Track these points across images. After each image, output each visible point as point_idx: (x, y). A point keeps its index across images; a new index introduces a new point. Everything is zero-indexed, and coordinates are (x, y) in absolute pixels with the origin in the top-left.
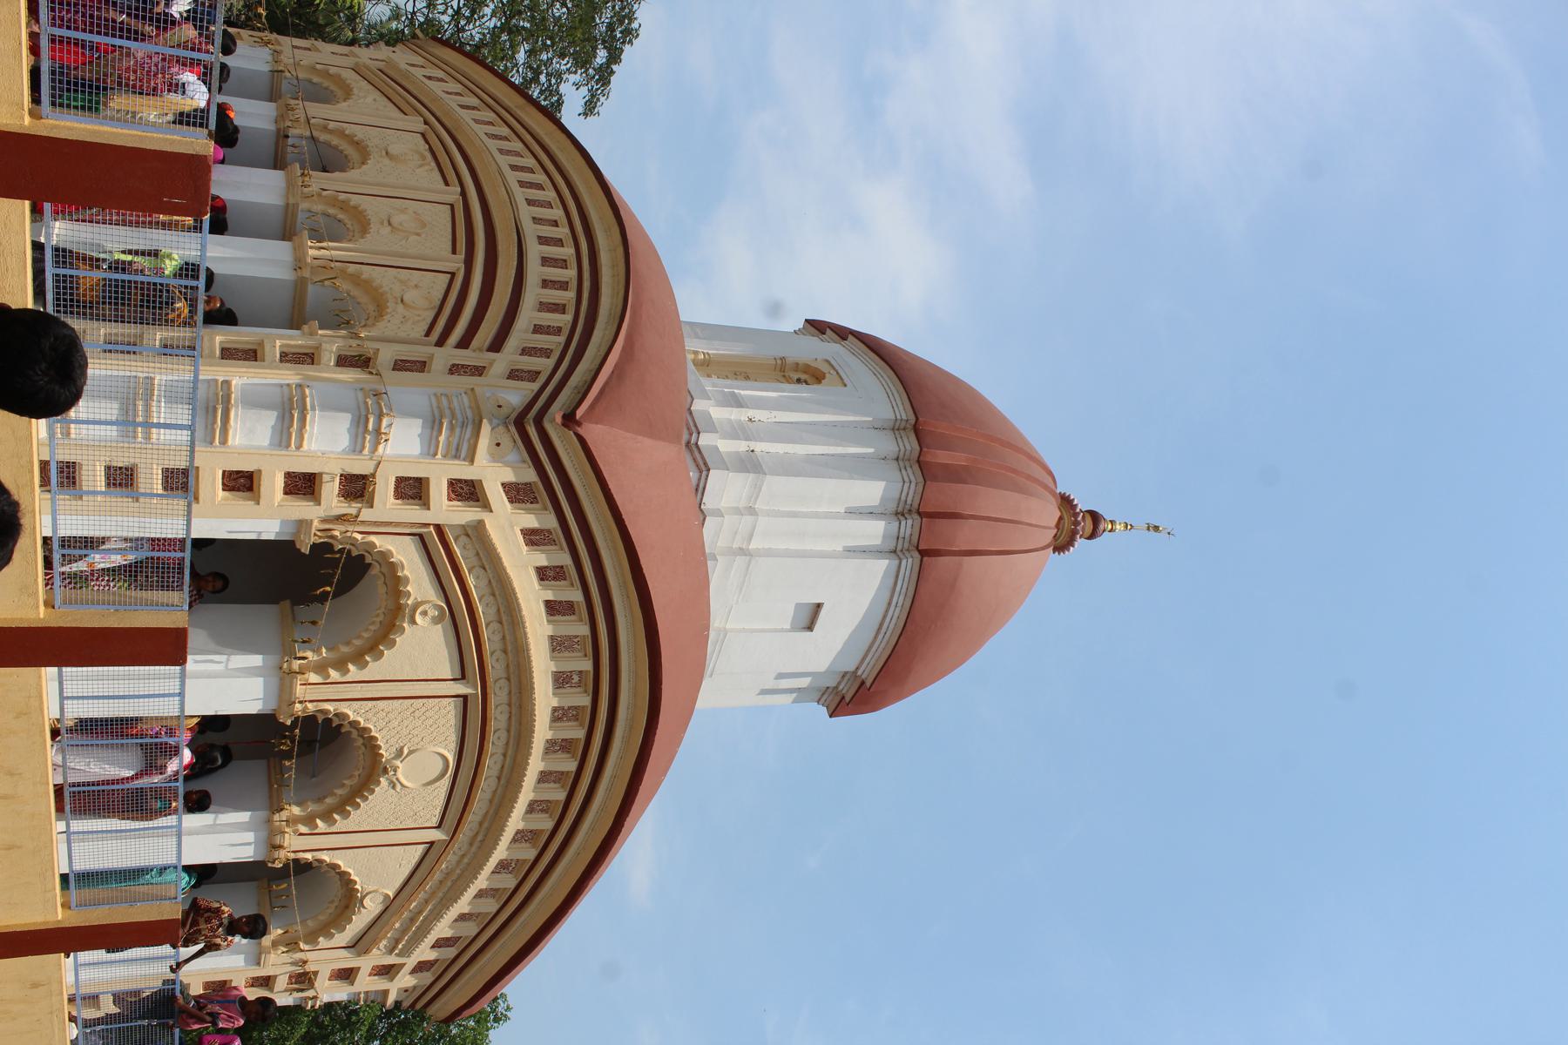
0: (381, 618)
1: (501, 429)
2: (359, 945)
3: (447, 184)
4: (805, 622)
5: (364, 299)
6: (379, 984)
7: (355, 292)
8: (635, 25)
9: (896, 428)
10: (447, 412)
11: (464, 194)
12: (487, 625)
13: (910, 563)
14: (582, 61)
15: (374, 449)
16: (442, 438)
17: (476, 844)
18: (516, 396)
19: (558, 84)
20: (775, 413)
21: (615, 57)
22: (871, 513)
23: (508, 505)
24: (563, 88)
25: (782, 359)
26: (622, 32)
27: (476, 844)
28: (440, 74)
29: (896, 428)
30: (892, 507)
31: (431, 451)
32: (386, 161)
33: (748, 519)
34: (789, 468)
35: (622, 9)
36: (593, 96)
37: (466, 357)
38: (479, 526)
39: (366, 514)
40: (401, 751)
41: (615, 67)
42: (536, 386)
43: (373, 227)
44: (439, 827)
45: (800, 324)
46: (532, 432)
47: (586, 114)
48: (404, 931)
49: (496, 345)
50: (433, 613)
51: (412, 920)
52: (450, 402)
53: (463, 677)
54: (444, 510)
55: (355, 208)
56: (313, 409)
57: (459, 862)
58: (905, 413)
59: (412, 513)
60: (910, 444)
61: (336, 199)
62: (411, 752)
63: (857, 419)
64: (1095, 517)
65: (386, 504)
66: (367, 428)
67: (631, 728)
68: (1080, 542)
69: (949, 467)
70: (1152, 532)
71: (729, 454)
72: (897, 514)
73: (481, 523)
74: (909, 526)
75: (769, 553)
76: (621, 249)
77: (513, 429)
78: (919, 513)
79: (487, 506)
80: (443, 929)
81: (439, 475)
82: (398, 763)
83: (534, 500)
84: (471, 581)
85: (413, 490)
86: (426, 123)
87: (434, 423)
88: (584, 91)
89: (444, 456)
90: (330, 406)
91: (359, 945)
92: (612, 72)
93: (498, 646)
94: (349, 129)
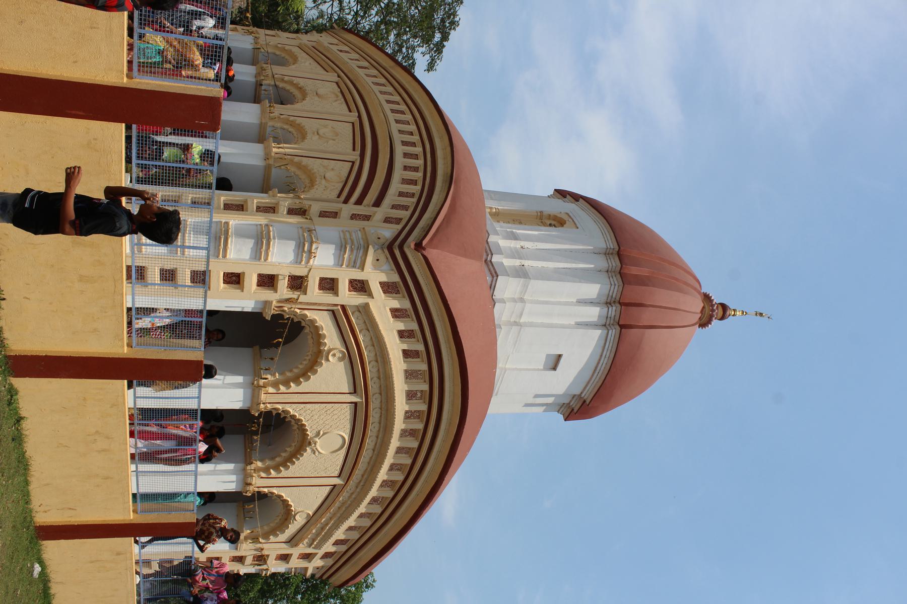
0: (309, 357)
1: (380, 251)
2: (292, 541)
3: (350, 111)
5: (303, 177)
7: (298, 172)
8: (457, 19)
9: (607, 253)
10: (349, 241)
11: (360, 117)
13: (614, 332)
14: (427, 40)
15: (308, 262)
16: (346, 256)
17: (360, 487)
18: (388, 232)
19: (413, 53)
20: (536, 243)
21: (445, 37)
22: (592, 303)
25: (541, 212)
26: (449, 23)
27: (360, 487)
28: (347, 49)
29: (607, 253)
30: (604, 299)
32: (316, 98)
33: (519, 305)
35: (450, 10)
36: (433, 60)
37: (361, 210)
38: (366, 306)
39: (303, 298)
40: (318, 433)
41: (445, 43)
42: (399, 227)
44: (339, 476)
48: (318, 535)
49: (377, 203)
50: (339, 355)
51: (323, 529)
52: (351, 235)
53: (355, 392)
54: (346, 297)
55: (304, 166)
56: (274, 238)
57: (349, 497)
58: (612, 245)
59: (328, 298)
60: (615, 263)
64: (724, 307)
65: (314, 293)
66: (304, 250)
67: (450, 424)
68: (715, 322)
69: (636, 271)
70: (758, 317)
71: (510, 267)
72: (607, 303)
74: (614, 311)
75: (531, 325)
76: (449, 149)
79: (370, 295)
80: (339, 534)
82: (317, 439)
84: (361, 338)
85: (329, 285)
86: (339, 76)
88: (427, 57)
89: (347, 266)
90: (283, 237)
92: (444, 46)
94: (296, 80)
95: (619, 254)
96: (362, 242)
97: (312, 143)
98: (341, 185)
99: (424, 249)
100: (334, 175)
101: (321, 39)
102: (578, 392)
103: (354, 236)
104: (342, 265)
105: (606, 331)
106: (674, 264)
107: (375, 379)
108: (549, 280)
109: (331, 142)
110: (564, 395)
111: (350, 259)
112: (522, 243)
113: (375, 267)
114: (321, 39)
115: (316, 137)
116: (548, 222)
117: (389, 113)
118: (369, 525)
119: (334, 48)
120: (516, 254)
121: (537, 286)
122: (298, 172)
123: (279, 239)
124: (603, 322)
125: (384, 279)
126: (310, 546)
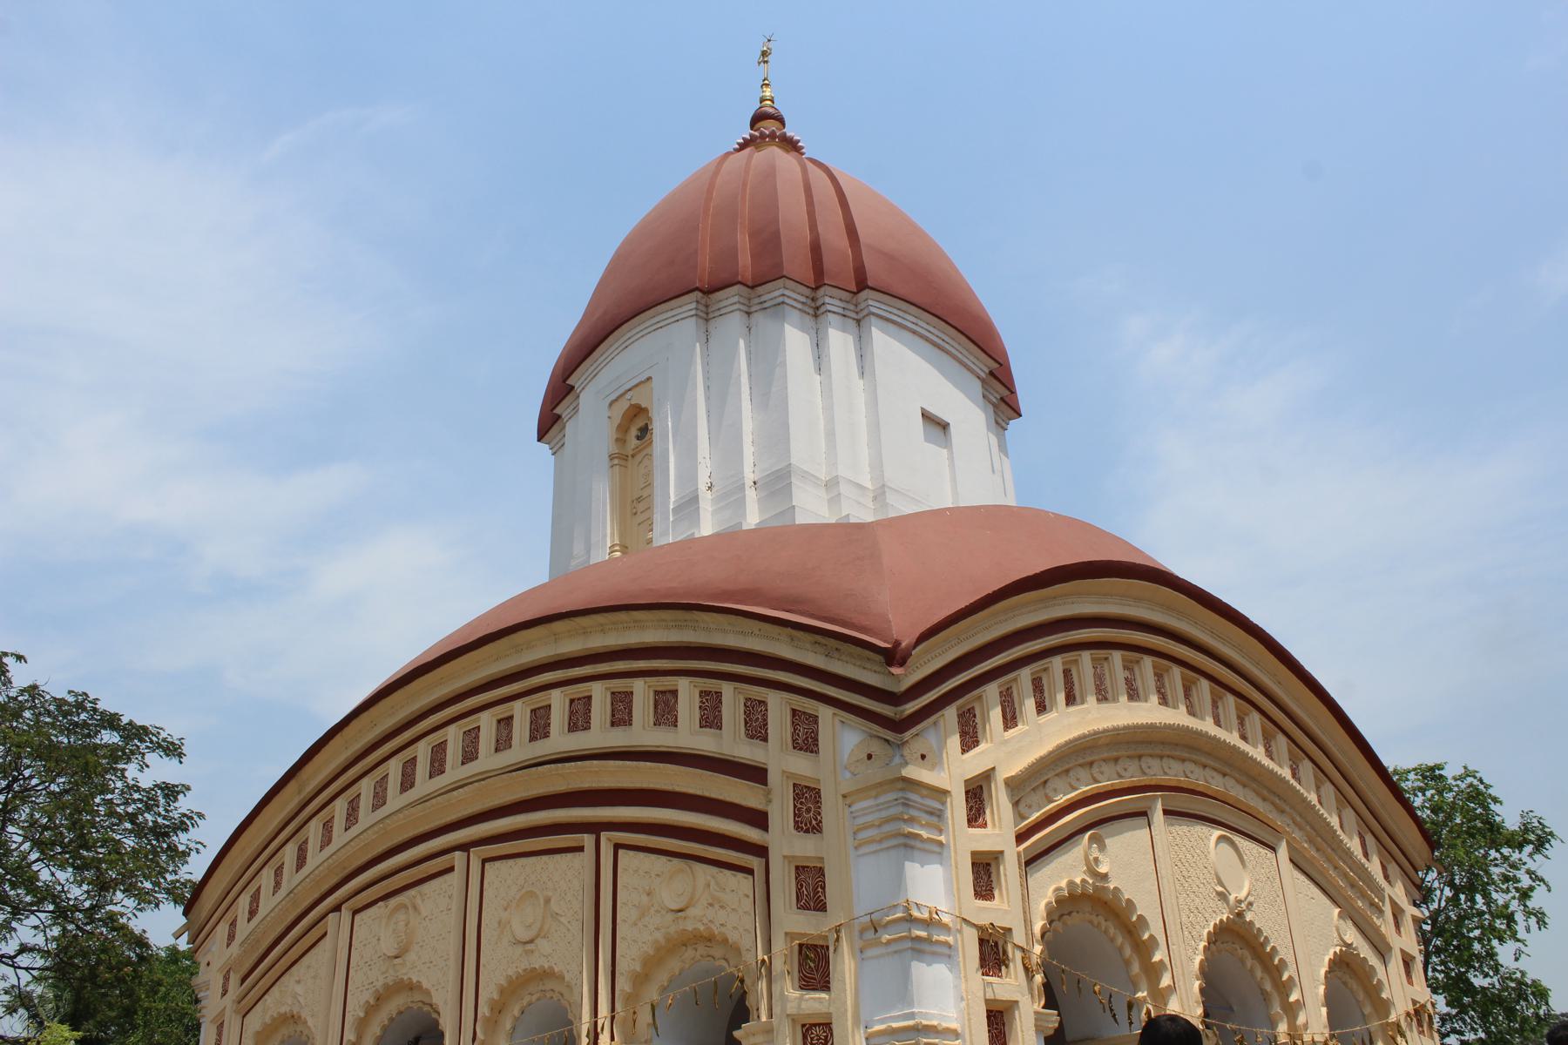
0: (1101, 919)
1: (906, 752)
2: (1382, 951)
3: (451, 869)
4: (937, 431)
5: (674, 965)
6: (1408, 927)
7: (662, 977)
8: (71, 699)
9: (706, 316)
10: (887, 828)
11: (465, 847)
12: (1097, 781)
13: (871, 300)
14: (117, 755)
15: (945, 927)
16: (924, 834)
17: (1284, 806)
18: (844, 739)
19: (138, 789)
20: (700, 459)
21: (111, 721)
22: (819, 345)
23: (982, 747)
24: (146, 782)
25: (611, 457)
26: (78, 713)
27: (1284, 806)
28: (244, 901)
29: (706, 316)
30: (808, 320)
31: (937, 850)
32: (411, 956)
33: (844, 488)
34: (777, 436)
35: (49, 713)
36: (160, 746)
37: (781, 811)
38: (1013, 785)
39: (1019, 937)
40: (1219, 894)
41: (125, 720)
42: (825, 713)
43: (538, 962)
44: (1273, 849)
45: (544, 448)
46: (911, 707)
47: (180, 755)
48: (1363, 896)
49: (757, 774)
50: (1095, 852)
51: (1353, 886)
52: (865, 827)
53: (1144, 814)
54: (999, 833)
55: (502, 991)
56: (912, 1016)
57: (1301, 829)
58: (688, 305)
59: (1010, 870)
60: (732, 296)
61: (487, 1020)
62: (1220, 883)
63: (699, 361)
64: (757, 119)
65: (1000, 911)
66: (918, 938)
67: (1169, 608)
68: (790, 131)
69: (757, 252)
70: (769, 58)
71: (761, 511)
72: (816, 316)
73: (1009, 783)
74: (831, 300)
75: (877, 465)
76: (558, 626)
77: (907, 735)
78: (817, 288)
79: (988, 775)
80: (1354, 845)
81: (966, 840)
82: (1232, 898)
83: (971, 711)
84: (1062, 799)
85: (984, 870)
86: (337, 908)
87: (909, 845)
88: (151, 758)
89: (941, 831)
90: (903, 991)
91: (1382, 951)
92: (131, 723)
93: (1108, 769)
94: (355, 1011)
95: (709, 291)
96: (891, 796)
97: (565, 952)
98: (700, 868)
99: (897, 644)
100: (661, 895)
101: (216, 965)
102: (977, 385)
103: (869, 818)
104: (940, 844)
105: (873, 319)
106: (710, 191)
107: (1119, 768)
108: (786, 426)
109: (554, 906)
110: (985, 411)
111: (928, 826)
112: (702, 487)
113: (936, 764)
114: (216, 965)
115: (543, 945)
116: (633, 442)
117: (413, 795)
118: (1331, 787)
119: (243, 929)
120: (732, 495)
121: (806, 451)
122: (662, 977)
123: (911, 1004)
124: (852, 324)
125: (955, 741)
126: (1381, 912)
